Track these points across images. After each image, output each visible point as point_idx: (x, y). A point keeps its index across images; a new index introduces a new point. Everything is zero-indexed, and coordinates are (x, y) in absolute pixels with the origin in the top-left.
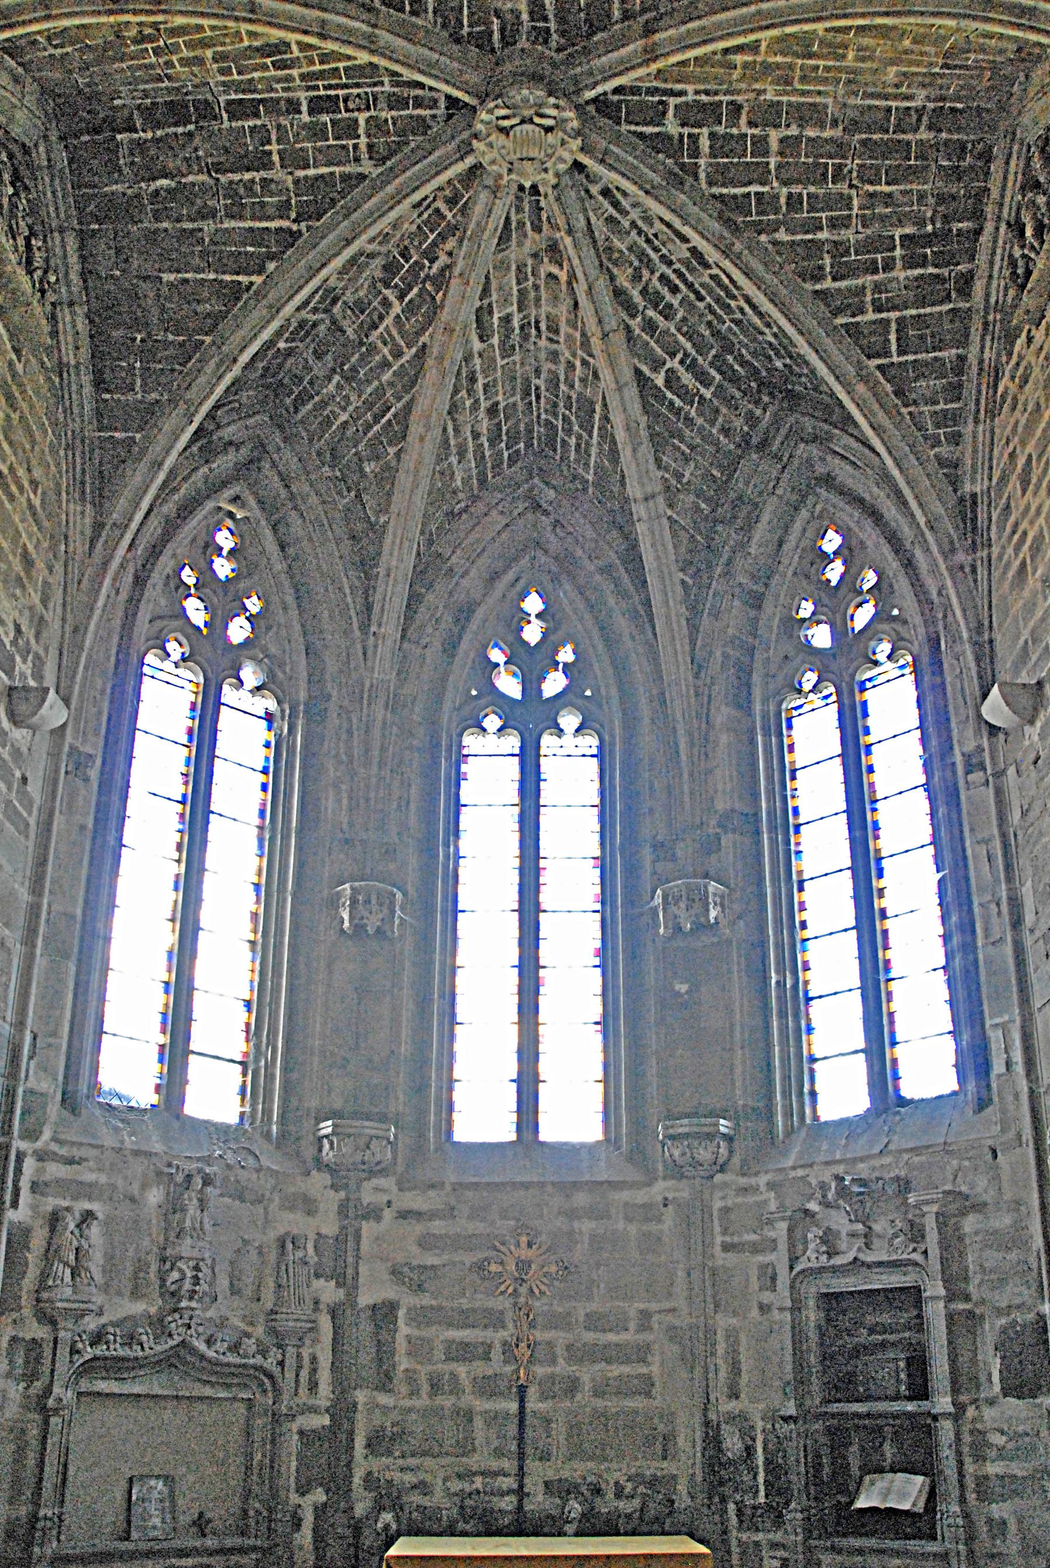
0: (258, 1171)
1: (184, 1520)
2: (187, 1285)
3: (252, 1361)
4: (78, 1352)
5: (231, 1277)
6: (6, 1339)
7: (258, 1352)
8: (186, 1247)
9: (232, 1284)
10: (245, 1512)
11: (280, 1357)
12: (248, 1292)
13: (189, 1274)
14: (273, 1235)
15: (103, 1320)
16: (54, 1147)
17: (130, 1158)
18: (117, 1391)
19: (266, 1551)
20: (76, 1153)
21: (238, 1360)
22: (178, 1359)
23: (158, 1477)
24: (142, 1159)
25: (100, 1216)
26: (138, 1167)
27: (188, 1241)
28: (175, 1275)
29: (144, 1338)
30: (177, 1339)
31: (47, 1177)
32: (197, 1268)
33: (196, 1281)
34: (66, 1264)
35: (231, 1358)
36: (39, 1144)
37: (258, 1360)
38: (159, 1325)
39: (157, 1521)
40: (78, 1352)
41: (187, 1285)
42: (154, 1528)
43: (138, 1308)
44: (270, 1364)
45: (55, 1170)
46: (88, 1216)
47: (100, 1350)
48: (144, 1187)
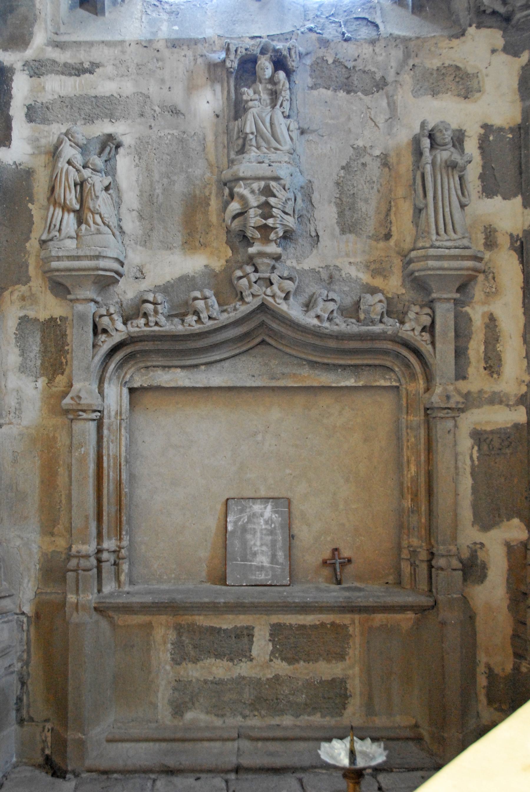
0: (373, 42)
1: (311, 558)
2: (254, 219)
3: (378, 328)
4: (105, 331)
5: (340, 203)
6: (12, 324)
7: (389, 313)
8: (247, 166)
9: (341, 214)
10: (399, 548)
11: (426, 320)
12: (371, 226)
13: (253, 201)
14: (403, 136)
15: (144, 285)
16: (53, 54)
17: (166, 53)
18: (187, 383)
19: (421, 610)
20: (83, 57)
21: (354, 328)
22: (262, 331)
23: (266, 500)
24: (185, 51)
25: (127, 140)
26: (179, 64)
27: (253, 154)
28: (235, 206)
29: (200, 304)
30: (253, 303)
31: (46, 98)
32: (268, 192)
33: (266, 209)
34: (65, 208)
35: (342, 325)
36: (30, 53)
37: (390, 326)
38: (226, 287)
39: (264, 560)
40: (105, 331)
41: (254, 219)
42: (261, 568)
43: (194, 264)
44: (411, 330)
45: (56, 86)
46: (110, 144)
47: (138, 326)
48: (191, 88)
